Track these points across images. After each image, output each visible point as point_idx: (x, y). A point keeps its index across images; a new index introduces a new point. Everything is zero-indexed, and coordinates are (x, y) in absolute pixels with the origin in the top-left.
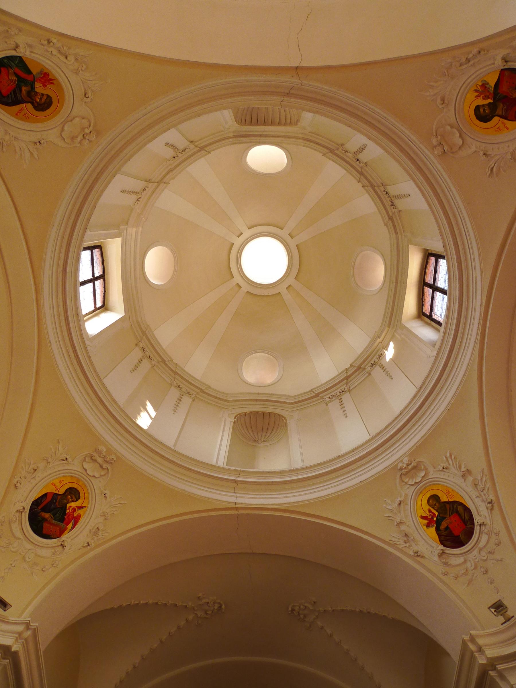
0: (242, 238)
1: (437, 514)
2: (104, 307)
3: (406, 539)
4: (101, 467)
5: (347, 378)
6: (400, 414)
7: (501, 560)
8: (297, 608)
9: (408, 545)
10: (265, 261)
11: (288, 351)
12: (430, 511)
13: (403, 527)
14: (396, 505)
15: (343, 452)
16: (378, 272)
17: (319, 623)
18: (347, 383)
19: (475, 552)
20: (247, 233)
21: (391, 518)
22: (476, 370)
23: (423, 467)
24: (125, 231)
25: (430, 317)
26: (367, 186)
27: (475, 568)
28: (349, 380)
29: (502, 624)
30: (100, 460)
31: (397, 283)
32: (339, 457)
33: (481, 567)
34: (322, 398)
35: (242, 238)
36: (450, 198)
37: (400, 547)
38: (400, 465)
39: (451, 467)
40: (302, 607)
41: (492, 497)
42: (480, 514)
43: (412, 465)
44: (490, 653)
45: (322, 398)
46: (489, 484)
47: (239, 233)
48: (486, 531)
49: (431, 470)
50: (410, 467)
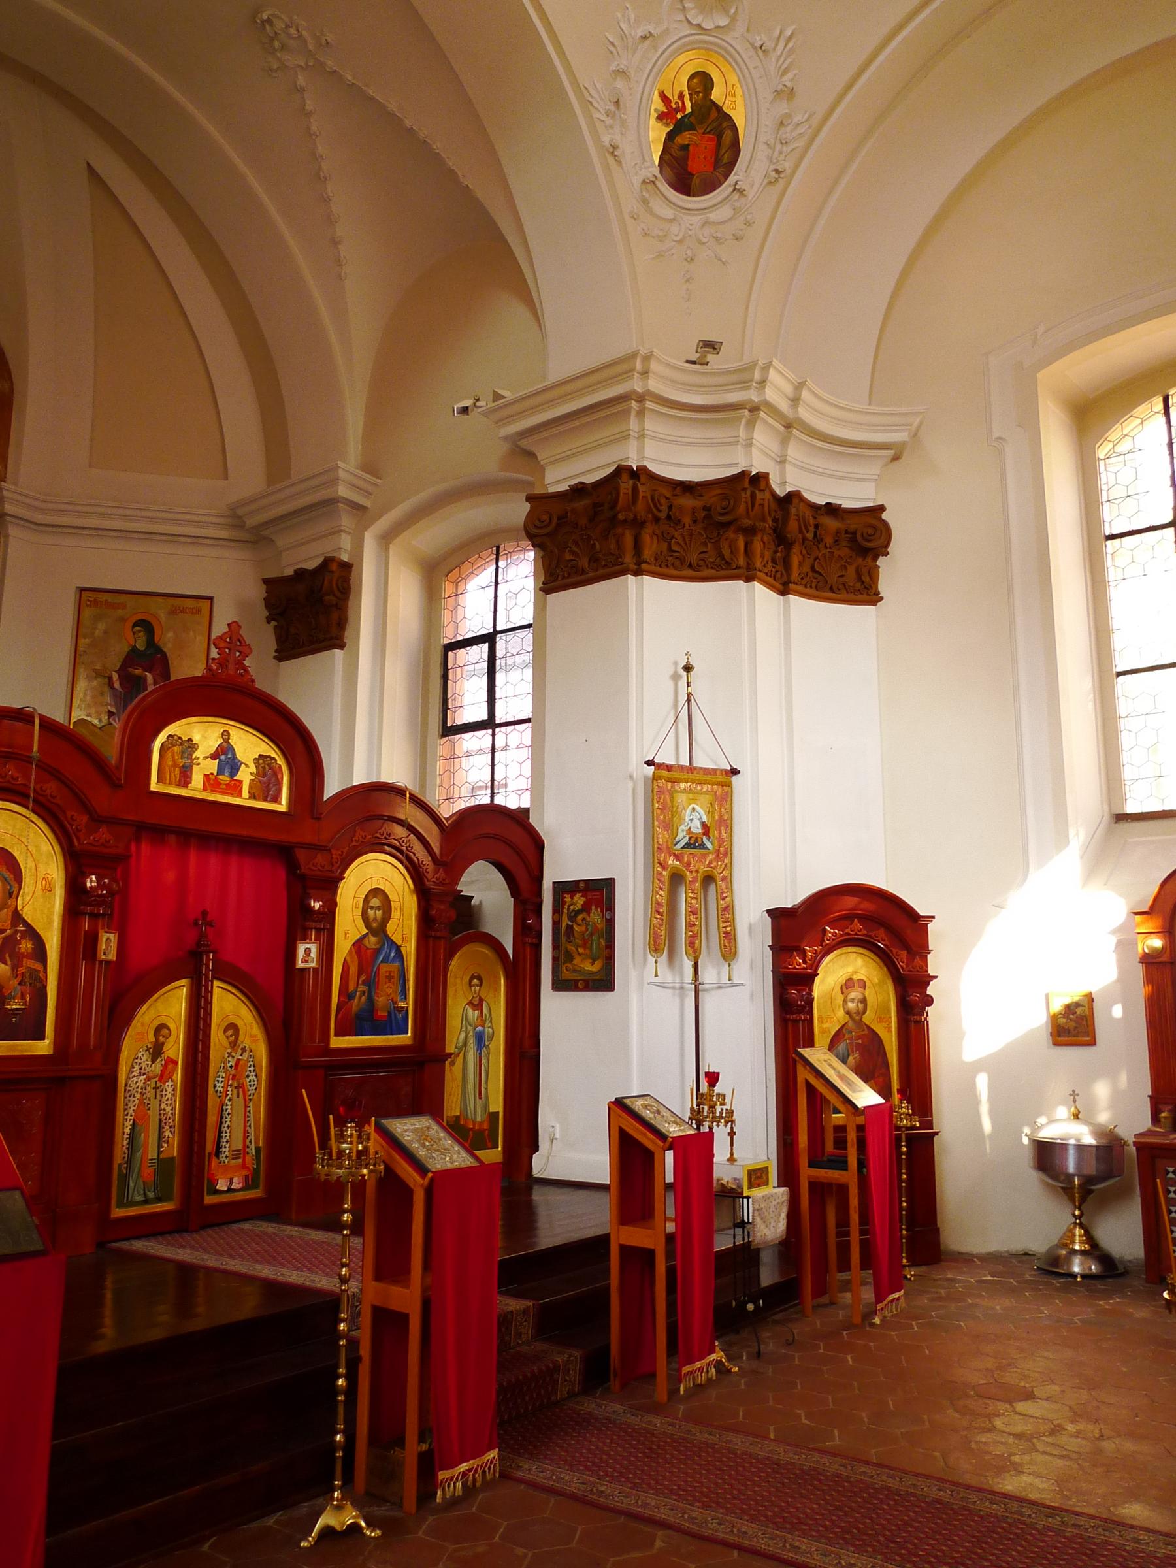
1: (689, 110)
3: (613, 109)
7: (724, 263)
8: (279, 25)
9: (609, 121)
12: (681, 96)
13: (620, 84)
14: (640, 33)
17: (301, 81)
19: (696, 220)
21: (612, 49)
23: (733, 11)
27: (680, 242)
29: (688, 362)
33: (688, 248)
37: (596, 115)
39: (774, 57)
40: (293, 31)
41: (787, 166)
42: (750, 170)
44: (654, 385)
46: (801, 143)
48: (737, 204)
49: (740, 28)
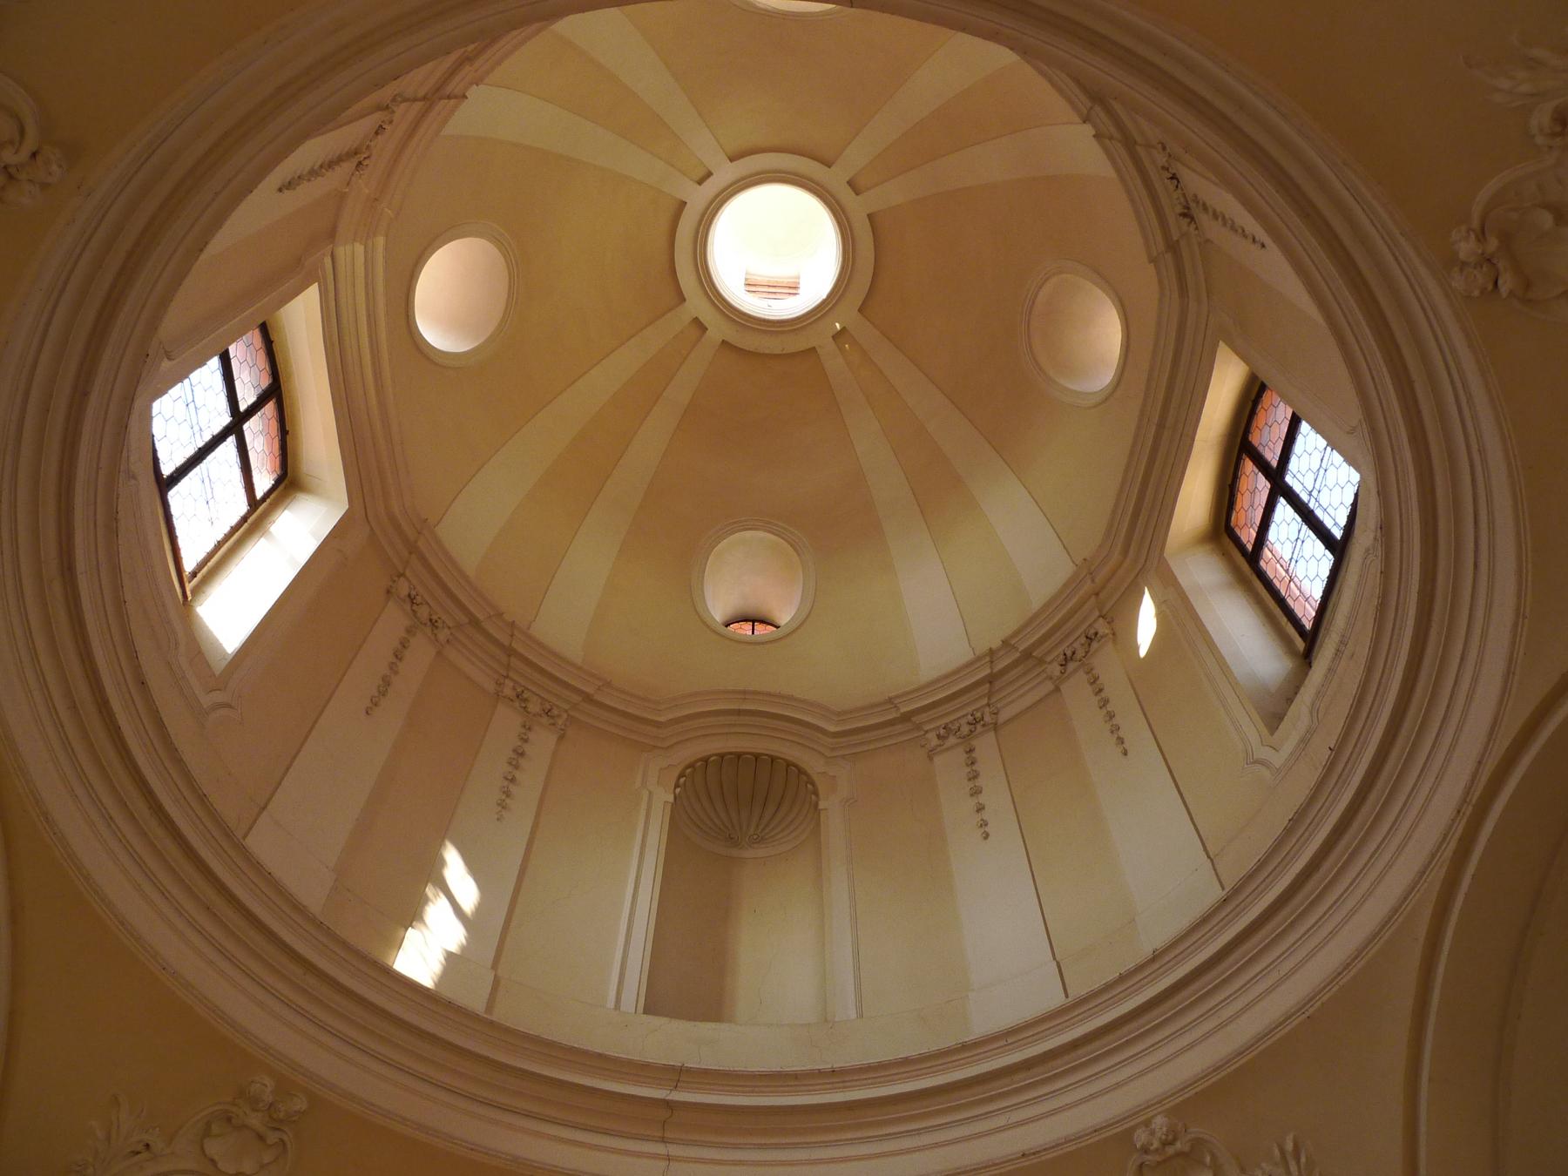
0: (711, 187)
2: (289, 482)
4: (261, 1138)
5: (990, 679)
6: (1153, 959)
10: (775, 249)
11: (831, 532)
15: (978, 1030)
16: (1101, 338)
18: (990, 695)
20: (726, 173)
22: (1422, 940)
23: (1208, 1159)
24: (328, 261)
25: (1253, 556)
26: (1111, 138)
28: (997, 685)
30: (255, 1121)
31: (1161, 425)
32: (964, 1047)
34: (918, 727)
35: (711, 187)
36: (1404, 280)
38: (1141, 1137)
43: (1178, 1145)
45: (918, 727)
47: (702, 173)
50: (1170, 1150)
